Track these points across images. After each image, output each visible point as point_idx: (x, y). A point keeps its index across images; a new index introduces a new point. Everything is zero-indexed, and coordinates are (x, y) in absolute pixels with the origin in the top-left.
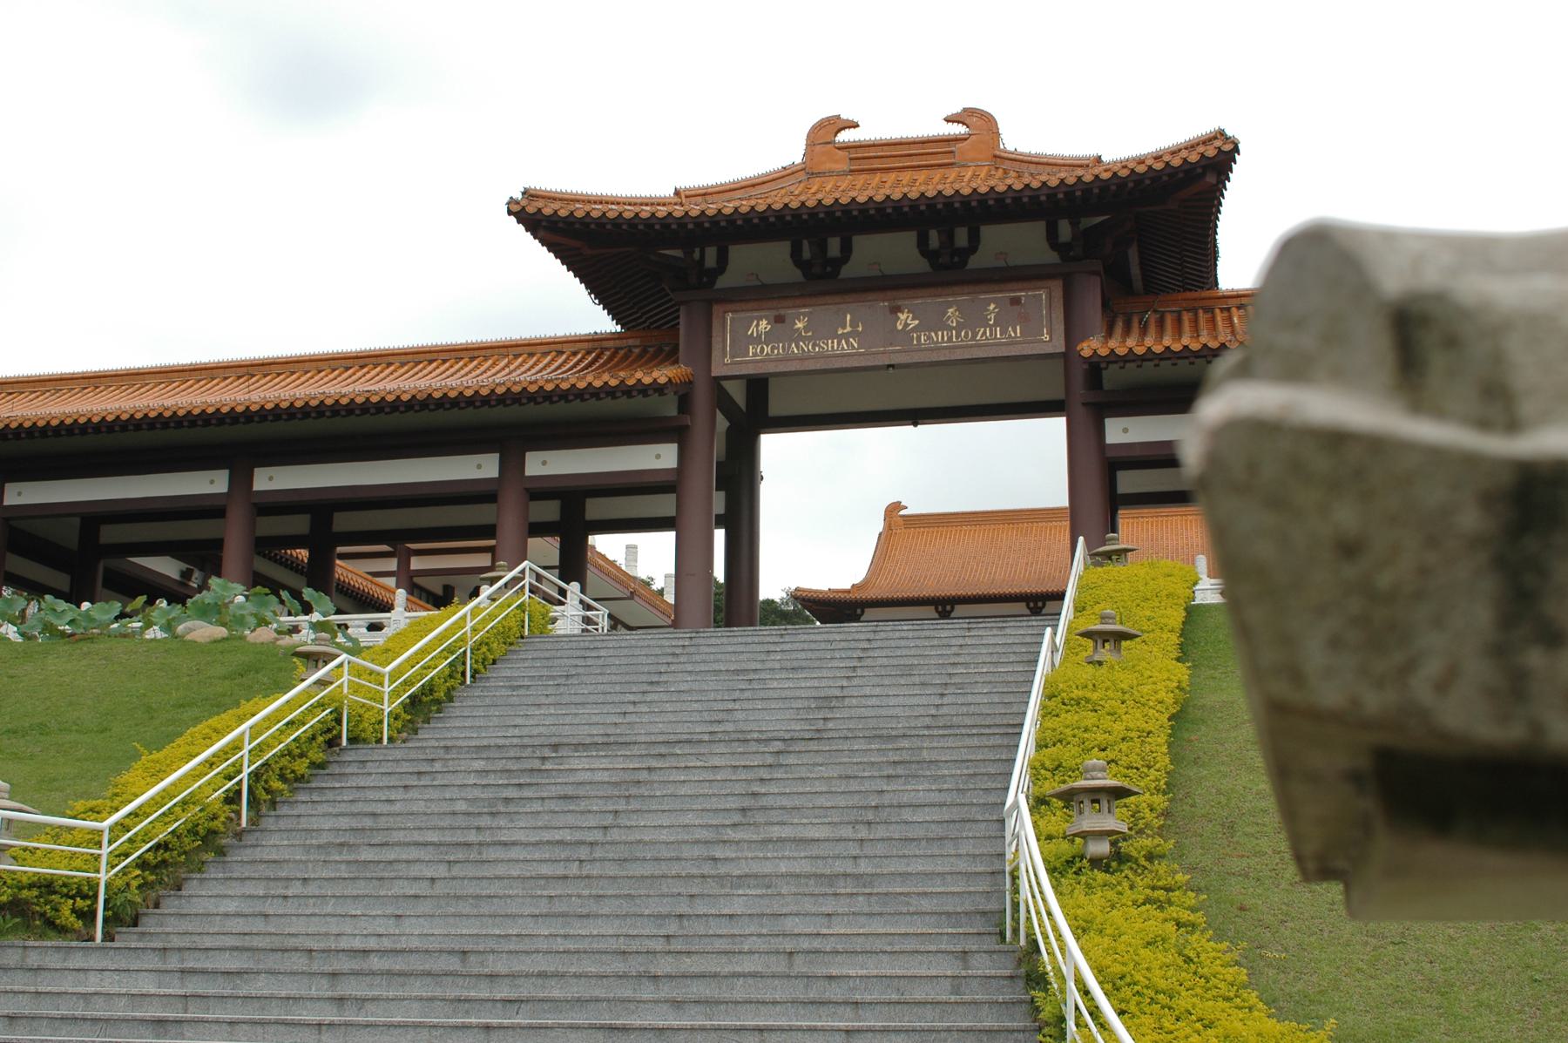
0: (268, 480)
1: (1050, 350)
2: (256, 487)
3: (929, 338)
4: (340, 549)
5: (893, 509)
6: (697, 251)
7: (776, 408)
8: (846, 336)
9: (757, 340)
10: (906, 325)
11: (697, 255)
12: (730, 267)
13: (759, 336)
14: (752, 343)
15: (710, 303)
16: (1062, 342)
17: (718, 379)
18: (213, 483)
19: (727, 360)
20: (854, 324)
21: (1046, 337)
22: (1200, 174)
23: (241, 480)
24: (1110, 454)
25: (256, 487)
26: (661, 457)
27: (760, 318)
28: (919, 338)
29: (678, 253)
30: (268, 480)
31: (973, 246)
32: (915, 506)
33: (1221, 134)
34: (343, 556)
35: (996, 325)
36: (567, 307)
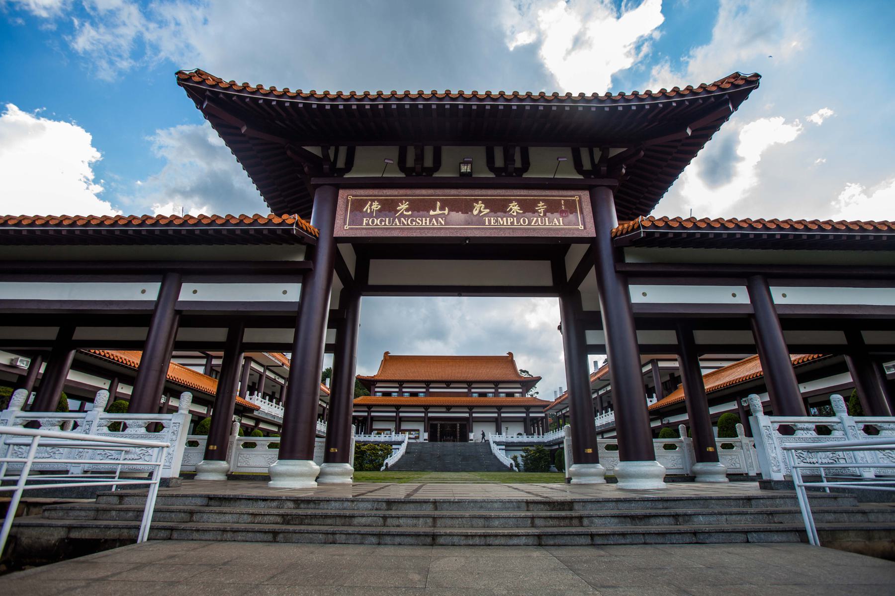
0: (193, 293)
1: (585, 235)
2: (181, 298)
3: (497, 221)
4: (706, 356)
6: (343, 151)
7: (372, 281)
8: (436, 217)
9: (370, 215)
10: (480, 212)
13: (372, 212)
14: (360, 217)
15: (338, 187)
18: (733, 296)
19: (347, 227)
20: (442, 209)
21: (581, 227)
23: (169, 293)
24: (635, 311)
25: (181, 298)
27: (373, 201)
28: (490, 221)
30: (193, 293)
34: (702, 360)
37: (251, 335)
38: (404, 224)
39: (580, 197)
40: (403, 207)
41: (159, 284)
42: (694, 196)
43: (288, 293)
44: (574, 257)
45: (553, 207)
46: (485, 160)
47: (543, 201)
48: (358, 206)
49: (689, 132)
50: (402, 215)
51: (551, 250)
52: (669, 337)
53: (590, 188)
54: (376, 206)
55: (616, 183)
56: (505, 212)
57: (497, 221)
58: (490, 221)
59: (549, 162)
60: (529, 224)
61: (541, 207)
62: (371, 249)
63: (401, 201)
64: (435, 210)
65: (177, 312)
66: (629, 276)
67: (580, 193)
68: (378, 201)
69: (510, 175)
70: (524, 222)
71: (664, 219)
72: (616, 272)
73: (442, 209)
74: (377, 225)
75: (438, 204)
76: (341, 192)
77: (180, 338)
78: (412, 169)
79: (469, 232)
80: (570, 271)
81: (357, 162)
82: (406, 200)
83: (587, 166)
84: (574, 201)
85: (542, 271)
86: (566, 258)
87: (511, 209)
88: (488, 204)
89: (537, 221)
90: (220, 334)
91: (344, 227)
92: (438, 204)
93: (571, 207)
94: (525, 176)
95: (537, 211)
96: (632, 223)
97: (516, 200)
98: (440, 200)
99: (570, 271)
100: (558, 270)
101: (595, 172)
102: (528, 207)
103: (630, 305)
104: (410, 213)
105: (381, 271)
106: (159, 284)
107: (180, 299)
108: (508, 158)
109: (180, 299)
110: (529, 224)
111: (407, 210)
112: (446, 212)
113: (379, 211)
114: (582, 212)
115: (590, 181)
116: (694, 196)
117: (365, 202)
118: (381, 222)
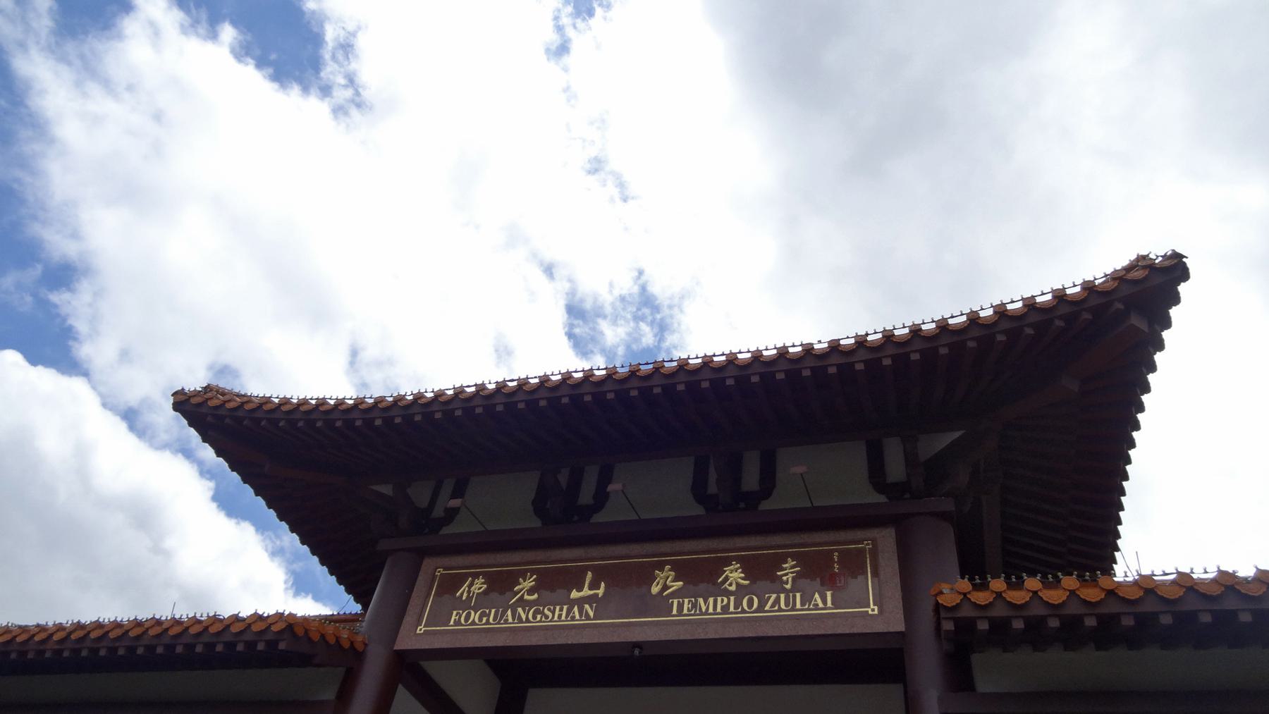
3: (694, 605)
8: (580, 602)
9: (465, 605)
10: (665, 587)
11: (563, 478)
13: (469, 598)
16: (900, 615)
19: (421, 629)
21: (873, 609)
28: (681, 606)
29: (387, 490)
31: (601, 498)
35: (794, 590)
36: (239, 566)
39: (874, 541)
45: (817, 571)
48: (451, 585)
54: (479, 586)
55: (948, 505)
57: (694, 605)
58: (681, 606)
59: (824, 473)
60: (761, 608)
61: (788, 572)
63: (523, 575)
64: (580, 589)
68: (485, 575)
73: (594, 586)
74: (473, 623)
75: (590, 574)
82: (533, 572)
83: (896, 470)
84: (862, 551)
87: (727, 578)
88: (682, 571)
89: (777, 601)
92: (590, 574)
93: (854, 565)
97: (738, 559)
104: (536, 596)
110: (761, 608)
111: (530, 592)
112: (601, 592)
114: (875, 574)
118: (480, 620)
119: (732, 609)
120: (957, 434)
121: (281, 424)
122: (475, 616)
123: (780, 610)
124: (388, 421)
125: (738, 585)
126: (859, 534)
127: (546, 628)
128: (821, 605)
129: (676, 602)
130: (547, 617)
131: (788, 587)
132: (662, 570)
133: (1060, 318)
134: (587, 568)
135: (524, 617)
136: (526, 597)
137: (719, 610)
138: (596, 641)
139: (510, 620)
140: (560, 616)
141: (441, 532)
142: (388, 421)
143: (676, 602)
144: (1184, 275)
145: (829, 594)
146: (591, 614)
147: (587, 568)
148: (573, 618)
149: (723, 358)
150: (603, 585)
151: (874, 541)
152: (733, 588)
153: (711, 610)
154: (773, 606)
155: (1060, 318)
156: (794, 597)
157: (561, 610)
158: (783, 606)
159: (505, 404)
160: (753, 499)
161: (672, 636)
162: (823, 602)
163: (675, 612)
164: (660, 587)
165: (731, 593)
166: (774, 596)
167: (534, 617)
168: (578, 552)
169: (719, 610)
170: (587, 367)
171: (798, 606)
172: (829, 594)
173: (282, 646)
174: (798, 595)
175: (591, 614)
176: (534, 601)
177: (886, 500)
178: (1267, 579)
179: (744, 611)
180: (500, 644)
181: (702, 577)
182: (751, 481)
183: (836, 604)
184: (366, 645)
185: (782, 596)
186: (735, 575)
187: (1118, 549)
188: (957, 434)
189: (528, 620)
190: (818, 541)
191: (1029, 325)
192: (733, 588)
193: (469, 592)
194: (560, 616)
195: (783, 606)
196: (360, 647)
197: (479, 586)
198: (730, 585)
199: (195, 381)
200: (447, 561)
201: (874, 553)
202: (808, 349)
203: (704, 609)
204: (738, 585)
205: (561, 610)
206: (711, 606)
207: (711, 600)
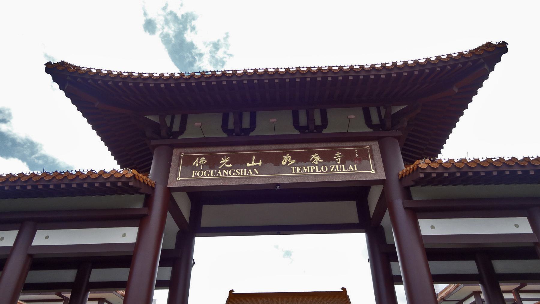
0: (45, 239)
1: (376, 178)
3: (302, 169)
5: (231, 291)
7: (204, 223)
8: (252, 168)
9: (198, 169)
10: (288, 162)
12: (257, 128)
13: (199, 166)
17: (170, 189)
19: (179, 179)
21: (373, 171)
22: (459, 78)
26: (127, 235)
27: (200, 157)
28: (296, 170)
30: (45, 239)
32: (236, 292)
33: (10, 115)
37: (97, 275)
38: (256, 174)
39: (371, 146)
40: (225, 161)
41: (16, 232)
42: (469, 141)
43: (127, 235)
44: (374, 197)
45: (348, 157)
46: (292, 121)
47: (340, 151)
48: (188, 161)
49: (456, 90)
50: (224, 167)
51: (357, 192)
52: (470, 267)
53: (378, 139)
54: (203, 161)
55: (399, 133)
56: (309, 161)
57: (302, 169)
58: (296, 170)
59: (346, 119)
60: (329, 170)
61: (338, 157)
62: (200, 197)
63: (223, 156)
64: (251, 163)
65: (30, 256)
66: (418, 212)
67: (371, 143)
68: (205, 156)
69: (312, 132)
70: (324, 169)
71: (451, 161)
72: (406, 208)
73: (257, 161)
74: (203, 176)
75: (254, 157)
76: (176, 151)
77: (127, 270)
78: (307, 127)
79: (358, 176)
80: (372, 208)
81: (189, 126)
82: (228, 155)
83: (375, 120)
84: (366, 150)
85: (348, 210)
86: (368, 198)
87: (313, 159)
88: (294, 156)
89: (335, 168)
90: (69, 275)
91: (178, 179)
92: (254, 157)
93: (363, 155)
94: (324, 131)
95: (335, 160)
96: (412, 166)
97: (317, 152)
98: (255, 154)
99: (372, 208)
100: (363, 208)
101: (382, 126)
102: (327, 157)
103: (420, 238)
104: (231, 165)
105: (210, 214)
106: (16, 232)
107: (33, 244)
108: (310, 118)
109: (33, 244)
110: (329, 170)
111: (228, 163)
112: (260, 164)
113: (206, 164)
114: (372, 159)
115: (380, 132)
116: (469, 141)
117: (194, 158)
118: (207, 174)
119: (317, 171)
120: (404, 106)
121: (100, 82)
122: (204, 173)
123: (337, 171)
124: (167, 86)
125: (318, 161)
126: (364, 143)
127: (296, 176)
128: (353, 170)
129: (293, 168)
130: (238, 174)
131: (339, 163)
132: (286, 156)
133: (461, 63)
134: (252, 154)
135: (227, 174)
136: (226, 166)
137: (312, 171)
138: (262, 183)
139: (221, 175)
140: (243, 173)
141: (250, 135)
142: (167, 86)
143: (293, 168)
144: (505, 50)
145: (355, 166)
146: (258, 173)
147: (252, 154)
148: (250, 174)
149: (263, 71)
150: (260, 161)
151: (371, 146)
152: (317, 163)
153: (309, 171)
154: (334, 170)
155: (461, 63)
156: (342, 167)
157: (243, 171)
158: (338, 170)
159: (248, 81)
160: (320, 129)
161: (294, 181)
162: (353, 168)
163: (294, 172)
164: (285, 162)
165: (316, 165)
166: (334, 166)
167: (232, 174)
168: (247, 148)
169: (312, 171)
170: (223, 70)
171: (344, 170)
172: (355, 166)
173: (131, 184)
174: (343, 166)
175: (258, 173)
176: (230, 167)
177: (227, 136)
178: (539, 159)
179: (322, 172)
180: (192, 185)
181: (303, 158)
182: (246, 124)
183: (358, 169)
184: (155, 185)
185: (337, 166)
186: (316, 158)
187: (440, 153)
188: (404, 106)
189: (229, 175)
190: (350, 145)
191: (449, 65)
192: (317, 163)
193: (199, 163)
194: (243, 173)
195: (338, 170)
196: (154, 186)
197: (203, 161)
198: (315, 162)
199: (56, 60)
200: (186, 150)
201: (371, 151)
202: (277, 71)
203: (306, 171)
204: (318, 161)
205: (243, 171)
206: (308, 170)
207: (308, 167)
